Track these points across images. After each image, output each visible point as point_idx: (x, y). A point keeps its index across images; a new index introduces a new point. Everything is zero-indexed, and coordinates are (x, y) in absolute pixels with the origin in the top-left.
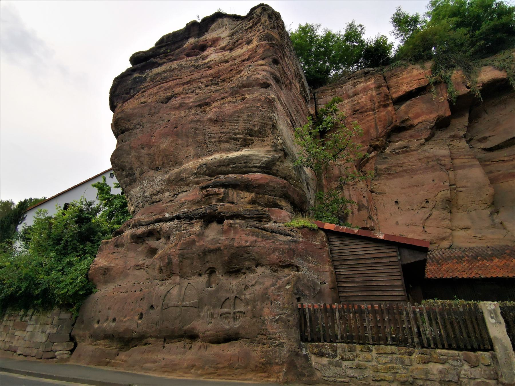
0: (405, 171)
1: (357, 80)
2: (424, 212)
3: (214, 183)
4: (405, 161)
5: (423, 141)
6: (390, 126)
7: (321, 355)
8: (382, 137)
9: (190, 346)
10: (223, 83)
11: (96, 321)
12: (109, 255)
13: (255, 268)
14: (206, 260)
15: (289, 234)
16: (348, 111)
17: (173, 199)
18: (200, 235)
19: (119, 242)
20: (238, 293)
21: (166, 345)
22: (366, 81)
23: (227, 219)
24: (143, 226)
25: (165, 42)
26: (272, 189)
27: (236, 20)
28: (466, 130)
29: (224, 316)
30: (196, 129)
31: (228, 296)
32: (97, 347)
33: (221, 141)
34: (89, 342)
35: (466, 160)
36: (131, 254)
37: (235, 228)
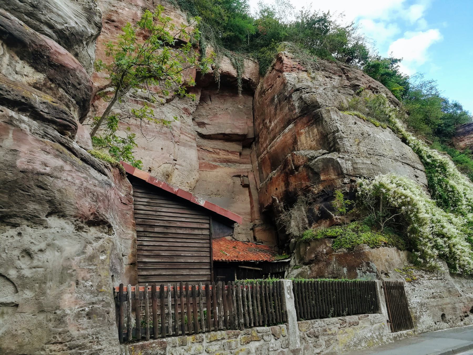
5: (164, 101)
13: (45, 218)
26: (76, 84)
35: (189, 139)
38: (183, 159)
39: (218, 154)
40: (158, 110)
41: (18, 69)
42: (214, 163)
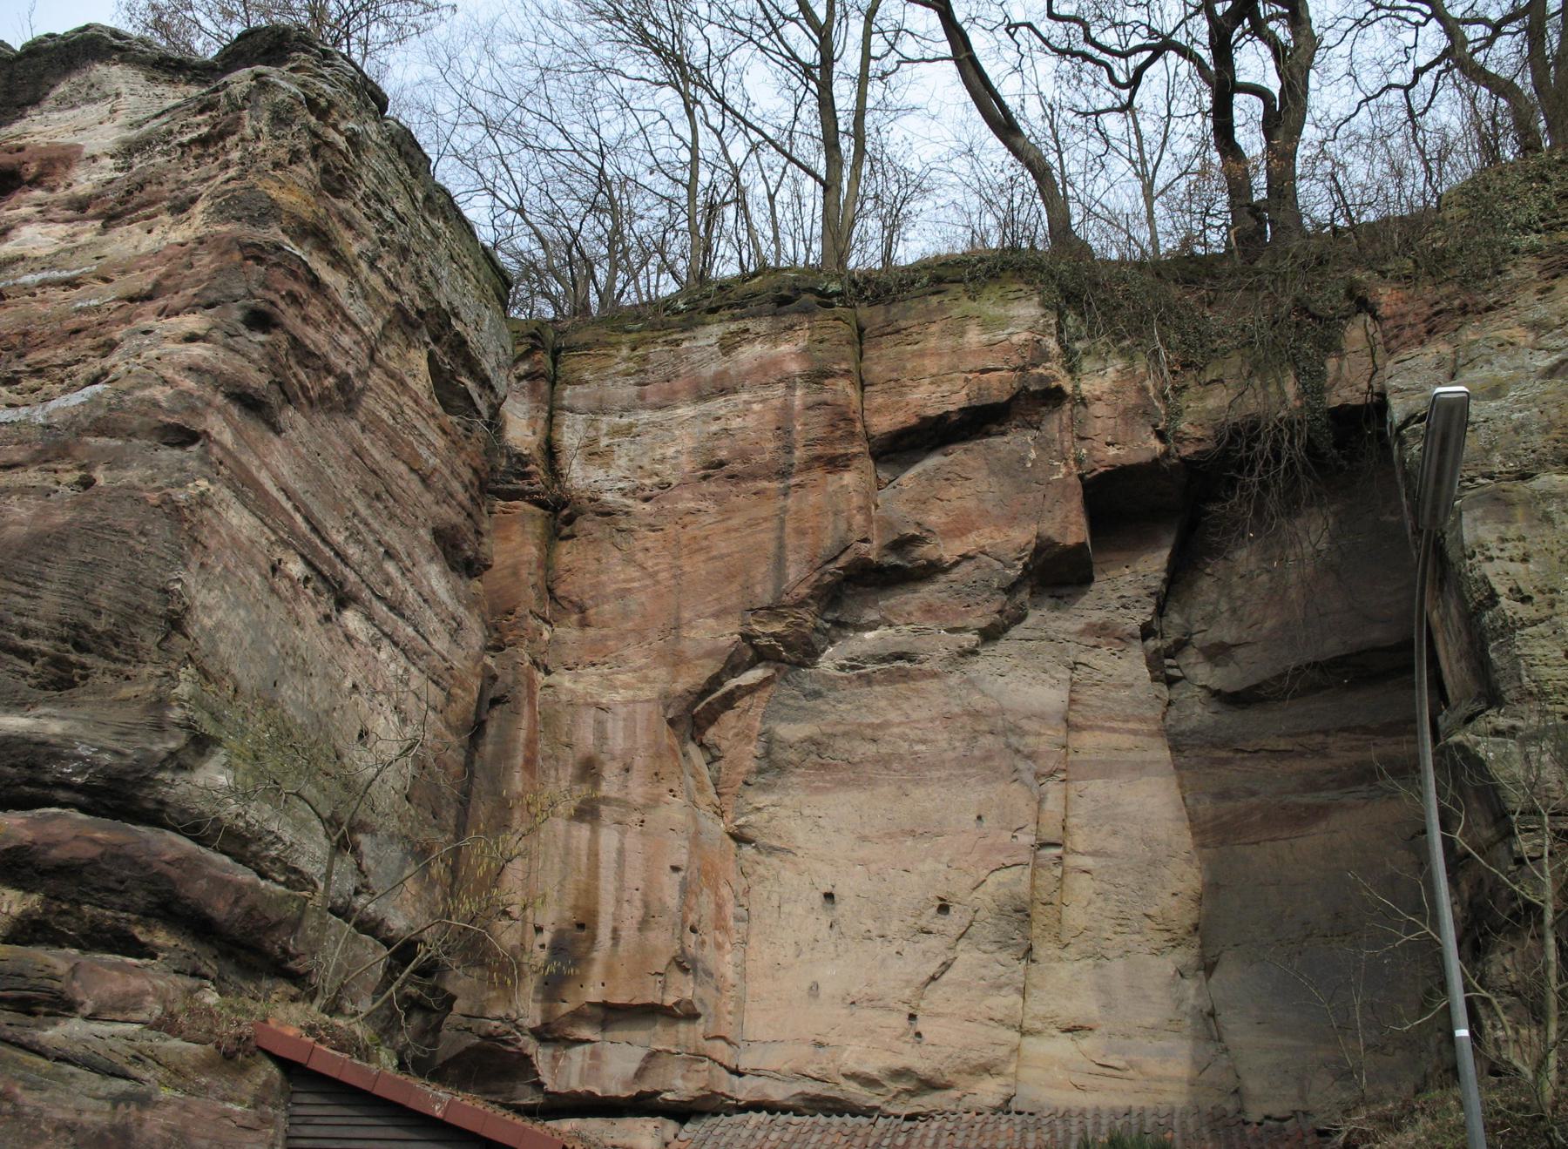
0: (884, 762)
2: (924, 953)
4: (893, 716)
6: (835, 558)
8: (801, 604)
10: (35, 382)
15: (122, 1069)
16: (683, 458)
22: (773, 337)
27: (167, 77)
28: (1150, 609)
38: (1107, 828)
39: (1322, 752)
40: (953, 680)
42: (1308, 799)
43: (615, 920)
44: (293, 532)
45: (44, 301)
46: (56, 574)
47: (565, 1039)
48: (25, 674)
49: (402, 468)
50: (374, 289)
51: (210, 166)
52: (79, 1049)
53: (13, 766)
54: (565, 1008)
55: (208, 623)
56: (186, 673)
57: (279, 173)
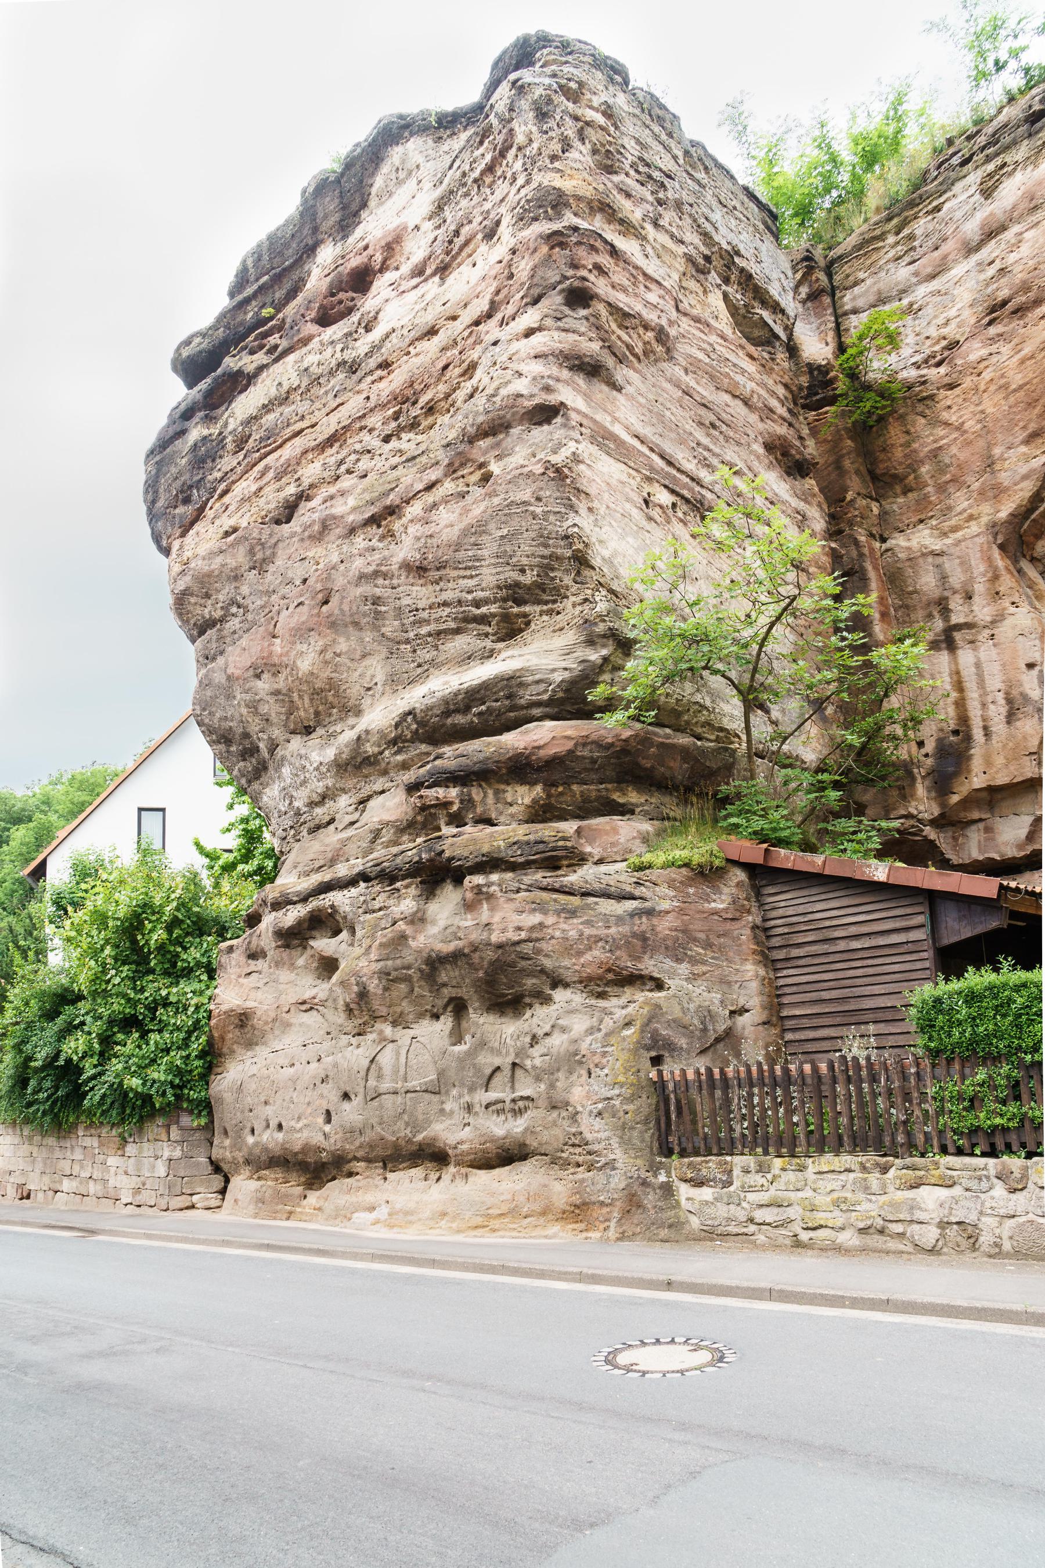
1: (998, 161)
3: (431, 774)
7: (699, 1183)
9: (438, 1174)
10: (430, 420)
11: (248, 1130)
12: (241, 980)
14: (440, 981)
17: (356, 816)
18: (418, 919)
19: (253, 945)
20: (517, 1055)
21: (389, 1175)
23: (471, 874)
24: (295, 903)
25: (252, 278)
27: (448, 132)
29: (494, 1107)
30: (377, 601)
31: (497, 1061)
32: (263, 1182)
33: (445, 631)
34: (248, 1173)
36: (285, 975)
37: (490, 897)
41: (509, 800)
43: (984, 720)
44: (652, 469)
45: (417, 355)
46: (485, 553)
47: (960, 822)
48: (487, 635)
49: (727, 398)
50: (663, 246)
51: (502, 188)
52: (597, 886)
53: (497, 701)
54: (955, 799)
55: (606, 553)
56: (601, 595)
57: (557, 164)
